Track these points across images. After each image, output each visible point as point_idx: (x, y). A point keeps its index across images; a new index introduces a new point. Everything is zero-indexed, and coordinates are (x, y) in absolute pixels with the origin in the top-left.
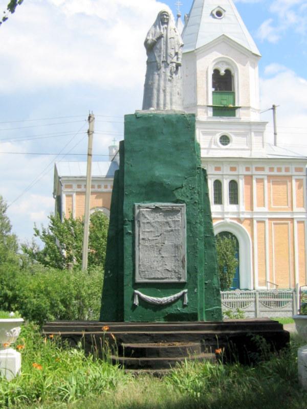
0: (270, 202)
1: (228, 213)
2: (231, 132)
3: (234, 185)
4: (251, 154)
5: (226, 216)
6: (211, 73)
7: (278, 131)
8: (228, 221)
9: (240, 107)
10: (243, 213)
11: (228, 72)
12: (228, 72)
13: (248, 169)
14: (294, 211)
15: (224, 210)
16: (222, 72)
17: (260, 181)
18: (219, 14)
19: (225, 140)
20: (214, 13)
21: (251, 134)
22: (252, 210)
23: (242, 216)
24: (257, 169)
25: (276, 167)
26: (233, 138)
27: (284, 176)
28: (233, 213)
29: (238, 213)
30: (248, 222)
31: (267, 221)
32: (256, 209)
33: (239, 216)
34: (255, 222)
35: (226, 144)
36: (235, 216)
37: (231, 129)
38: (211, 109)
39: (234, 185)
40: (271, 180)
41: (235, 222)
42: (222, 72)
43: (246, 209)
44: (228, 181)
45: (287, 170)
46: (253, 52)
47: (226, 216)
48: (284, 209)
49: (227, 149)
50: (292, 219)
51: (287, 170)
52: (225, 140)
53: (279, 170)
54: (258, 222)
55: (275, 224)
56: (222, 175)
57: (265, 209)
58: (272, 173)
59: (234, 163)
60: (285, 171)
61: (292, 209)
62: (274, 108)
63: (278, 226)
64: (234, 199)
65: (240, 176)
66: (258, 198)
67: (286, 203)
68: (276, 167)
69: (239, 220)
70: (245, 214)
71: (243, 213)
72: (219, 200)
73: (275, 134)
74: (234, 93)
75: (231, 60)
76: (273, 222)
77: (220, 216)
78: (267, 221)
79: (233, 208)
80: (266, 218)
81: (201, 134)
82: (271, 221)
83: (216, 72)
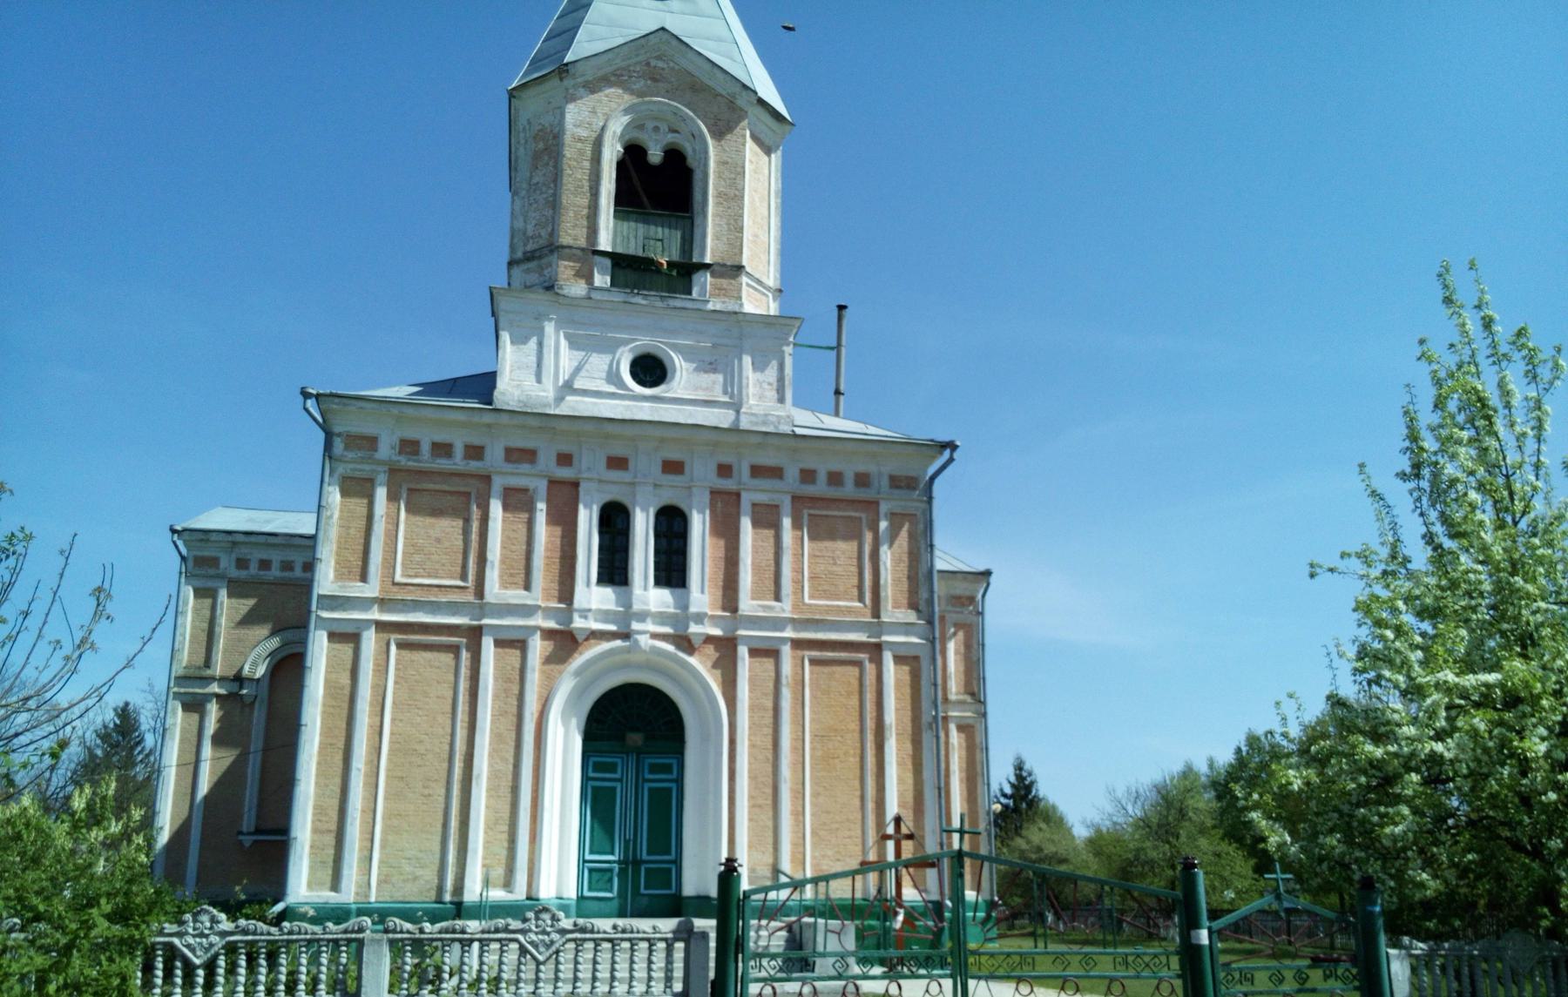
0: (799, 583)
1: (642, 616)
2: (675, 347)
4: (737, 419)
6: (611, 153)
10: (699, 618)
14: (885, 619)
15: (630, 606)
16: (655, 155)
17: (767, 518)
21: (740, 360)
22: (735, 610)
23: (694, 629)
24: (757, 471)
25: (253, 569)
26: (682, 369)
27: (852, 503)
28: (662, 618)
30: (710, 650)
31: (786, 650)
32: (747, 605)
33: (571, 621)
34: (743, 651)
37: (673, 333)
38: (608, 262)
39: (671, 526)
40: (806, 512)
41: (670, 648)
42: (655, 155)
43: (713, 607)
46: (761, 94)
47: (635, 626)
48: (849, 610)
52: (650, 370)
54: (754, 653)
55: (813, 662)
57: (785, 609)
58: (810, 490)
61: (876, 613)
63: (826, 669)
64: (672, 571)
66: (757, 568)
67: (855, 592)
68: (253, 569)
69: (684, 642)
70: (789, 628)
71: (699, 618)
72: (614, 571)
73: (62, 575)
74: (692, 219)
76: (808, 654)
78: (786, 650)
80: (783, 640)
81: (563, 343)
82: (800, 653)
83: (633, 154)
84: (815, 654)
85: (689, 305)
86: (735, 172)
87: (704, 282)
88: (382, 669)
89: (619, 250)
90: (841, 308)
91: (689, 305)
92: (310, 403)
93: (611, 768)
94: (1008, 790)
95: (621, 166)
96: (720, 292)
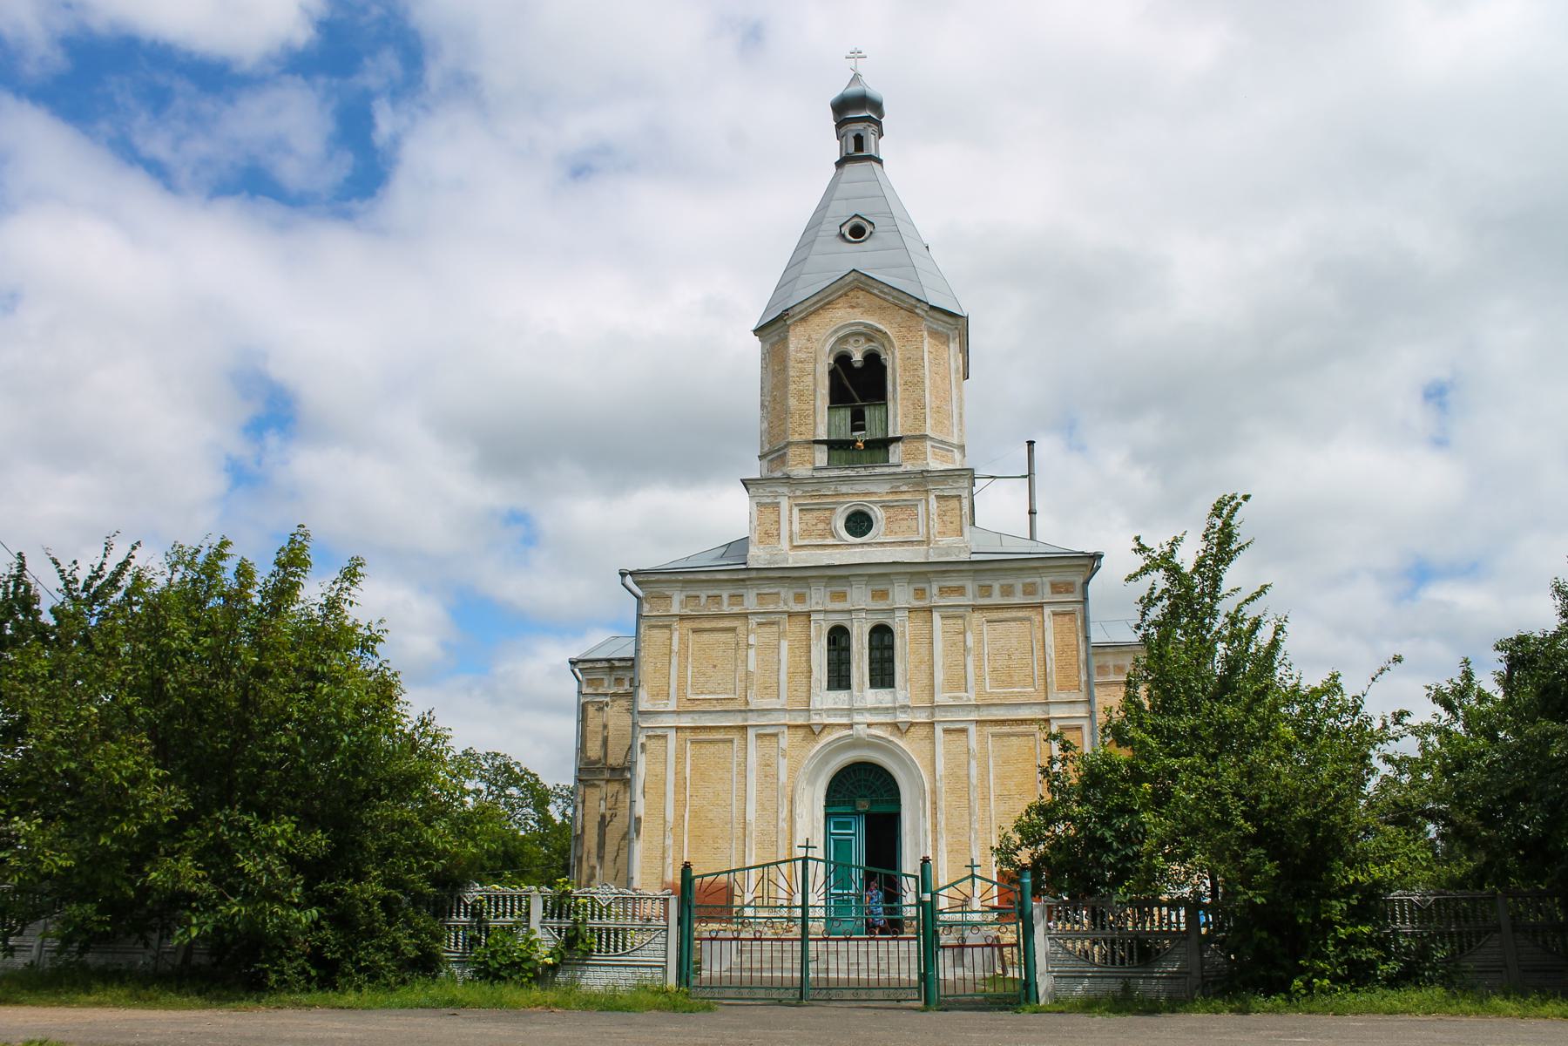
1: (860, 710)
3: (882, 636)
5: (857, 718)
7: (1038, 507)
8: (861, 731)
9: (897, 439)
11: (873, 359)
12: (873, 359)
13: (920, 593)
16: (857, 357)
18: (858, 232)
19: (859, 523)
20: (846, 230)
29: (850, 711)
31: (672, 735)
35: (863, 534)
36: (888, 719)
38: (825, 448)
42: (857, 357)
44: (867, 629)
45: (1030, 590)
49: (863, 544)
50: (745, 728)
51: (1030, 590)
52: (859, 523)
53: (1007, 591)
56: (850, 611)
57: (971, 697)
59: (880, 576)
60: (1025, 593)
62: (1031, 443)
64: (882, 675)
65: (897, 614)
73: (1032, 513)
75: (866, 325)
77: (845, 721)
79: (882, 696)
81: (796, 510)
83: (843, 360)
84: (997, 729)
85: (887, 470)
86: (914, 365)
87: (896, 453)
88: (680, 759)
89: (833, 437)
90: (1031, 443)
91: (887, 470)
92: (629, 579)
93: (847, 825)
94: (83, 575)
95: (833, 374)
96: (911, 456)
